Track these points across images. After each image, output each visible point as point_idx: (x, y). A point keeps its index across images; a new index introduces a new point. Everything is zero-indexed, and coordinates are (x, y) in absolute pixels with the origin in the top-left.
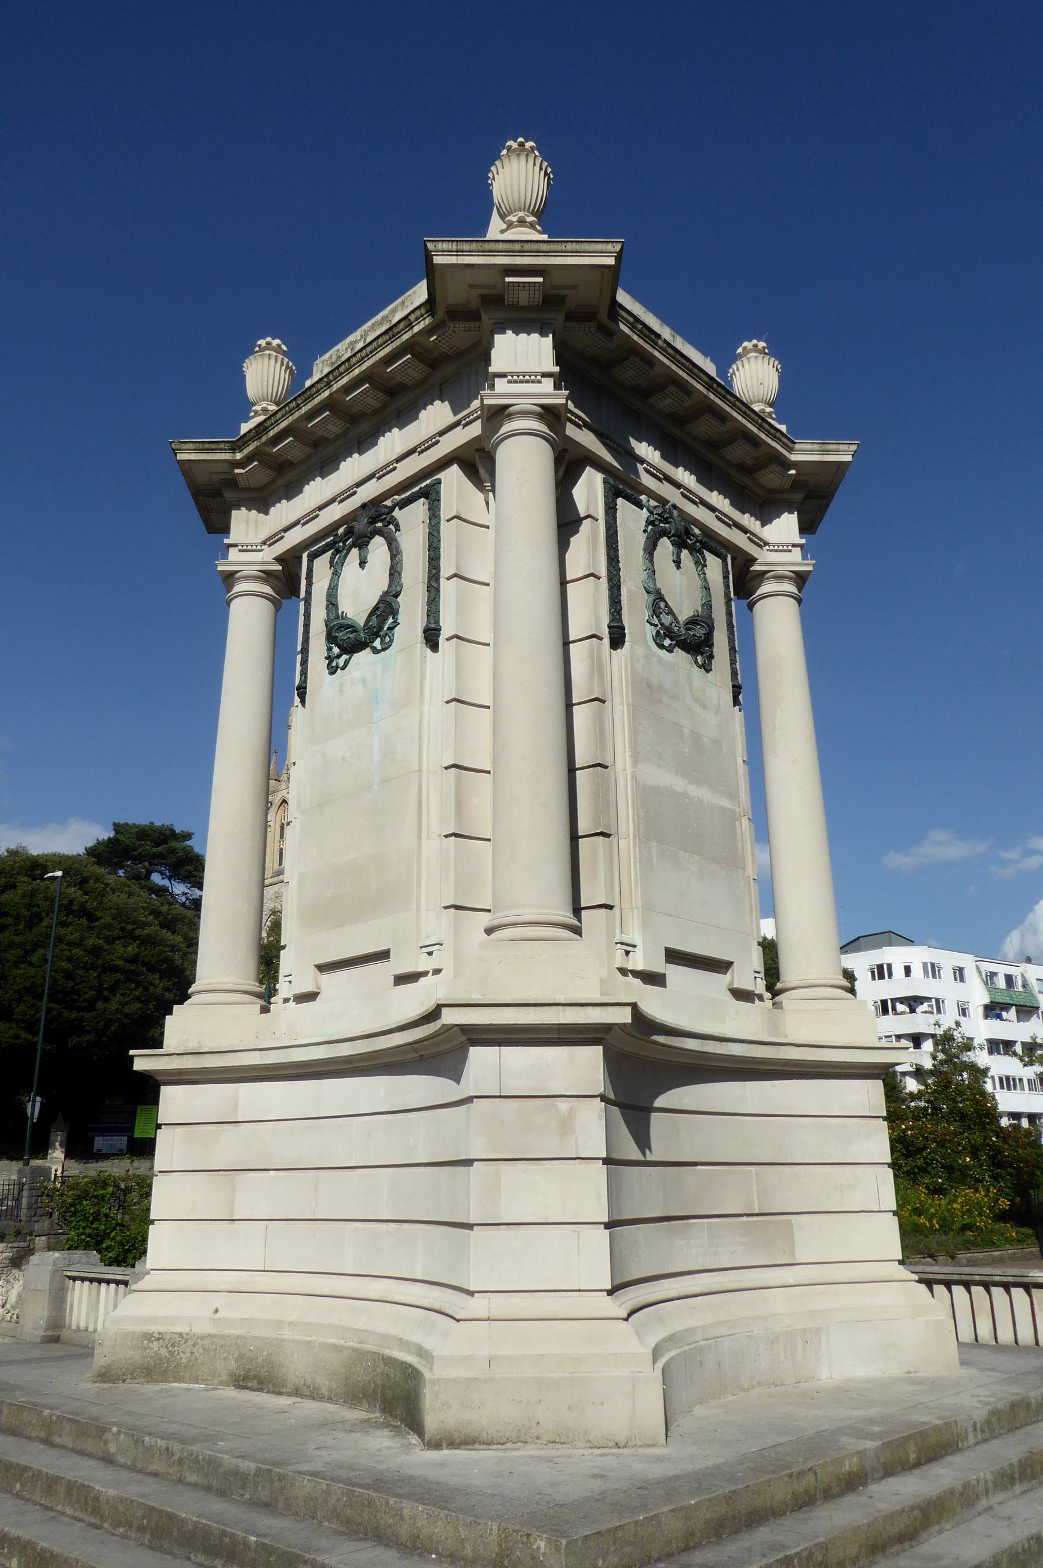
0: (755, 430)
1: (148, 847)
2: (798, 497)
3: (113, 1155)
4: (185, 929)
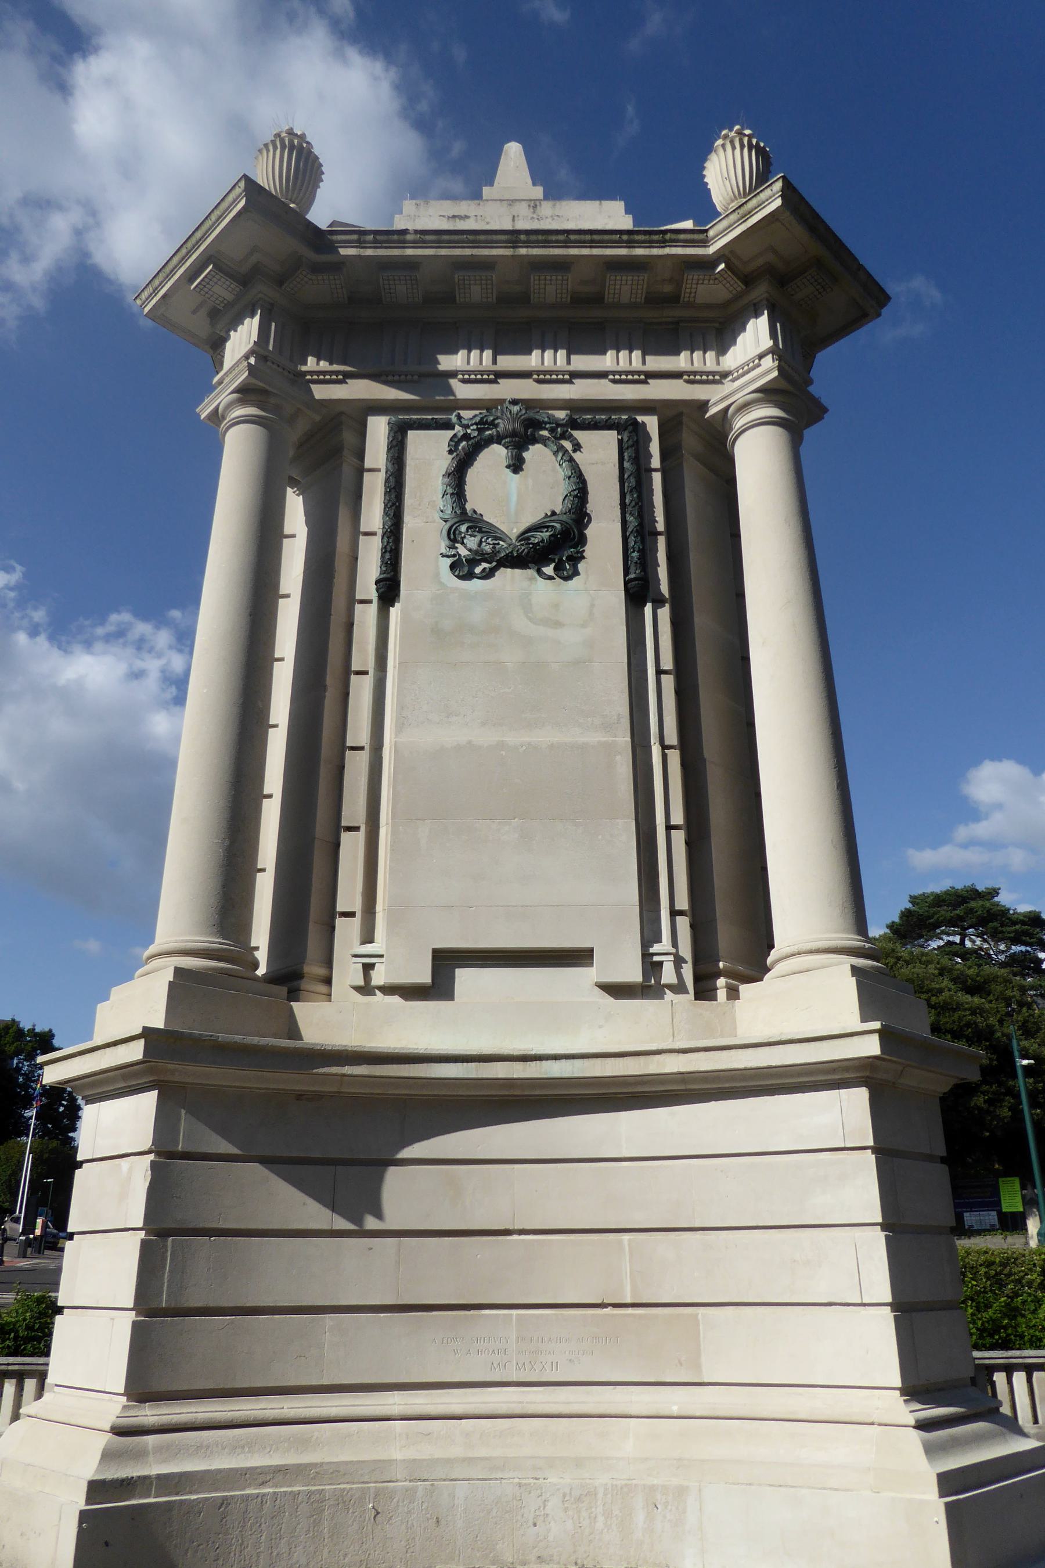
0: (623, 252)
1: (944, 912)
2: (761, 290)
3: (985, 1230)
4: (999, 988)
